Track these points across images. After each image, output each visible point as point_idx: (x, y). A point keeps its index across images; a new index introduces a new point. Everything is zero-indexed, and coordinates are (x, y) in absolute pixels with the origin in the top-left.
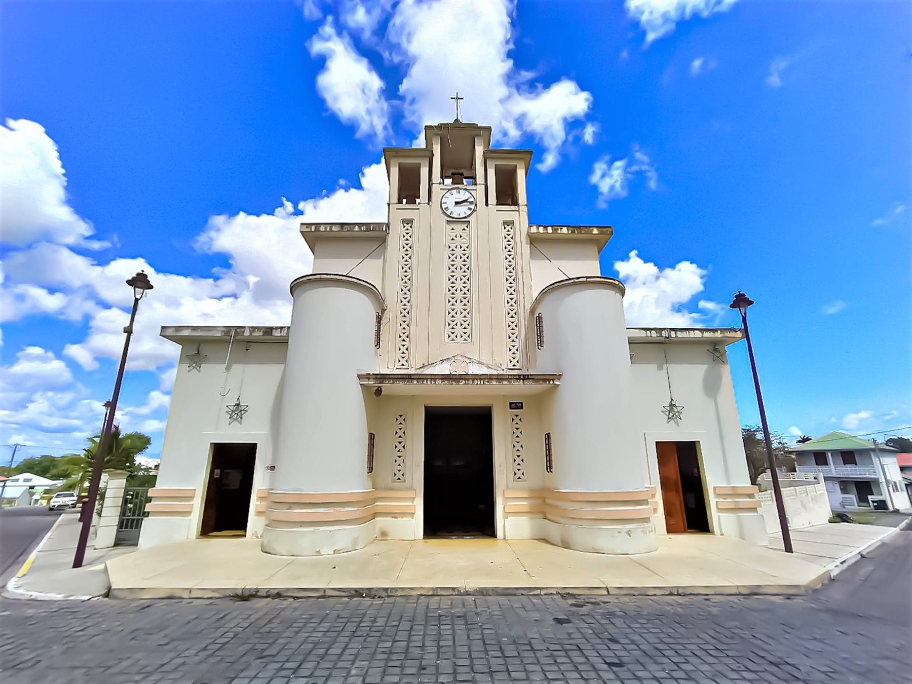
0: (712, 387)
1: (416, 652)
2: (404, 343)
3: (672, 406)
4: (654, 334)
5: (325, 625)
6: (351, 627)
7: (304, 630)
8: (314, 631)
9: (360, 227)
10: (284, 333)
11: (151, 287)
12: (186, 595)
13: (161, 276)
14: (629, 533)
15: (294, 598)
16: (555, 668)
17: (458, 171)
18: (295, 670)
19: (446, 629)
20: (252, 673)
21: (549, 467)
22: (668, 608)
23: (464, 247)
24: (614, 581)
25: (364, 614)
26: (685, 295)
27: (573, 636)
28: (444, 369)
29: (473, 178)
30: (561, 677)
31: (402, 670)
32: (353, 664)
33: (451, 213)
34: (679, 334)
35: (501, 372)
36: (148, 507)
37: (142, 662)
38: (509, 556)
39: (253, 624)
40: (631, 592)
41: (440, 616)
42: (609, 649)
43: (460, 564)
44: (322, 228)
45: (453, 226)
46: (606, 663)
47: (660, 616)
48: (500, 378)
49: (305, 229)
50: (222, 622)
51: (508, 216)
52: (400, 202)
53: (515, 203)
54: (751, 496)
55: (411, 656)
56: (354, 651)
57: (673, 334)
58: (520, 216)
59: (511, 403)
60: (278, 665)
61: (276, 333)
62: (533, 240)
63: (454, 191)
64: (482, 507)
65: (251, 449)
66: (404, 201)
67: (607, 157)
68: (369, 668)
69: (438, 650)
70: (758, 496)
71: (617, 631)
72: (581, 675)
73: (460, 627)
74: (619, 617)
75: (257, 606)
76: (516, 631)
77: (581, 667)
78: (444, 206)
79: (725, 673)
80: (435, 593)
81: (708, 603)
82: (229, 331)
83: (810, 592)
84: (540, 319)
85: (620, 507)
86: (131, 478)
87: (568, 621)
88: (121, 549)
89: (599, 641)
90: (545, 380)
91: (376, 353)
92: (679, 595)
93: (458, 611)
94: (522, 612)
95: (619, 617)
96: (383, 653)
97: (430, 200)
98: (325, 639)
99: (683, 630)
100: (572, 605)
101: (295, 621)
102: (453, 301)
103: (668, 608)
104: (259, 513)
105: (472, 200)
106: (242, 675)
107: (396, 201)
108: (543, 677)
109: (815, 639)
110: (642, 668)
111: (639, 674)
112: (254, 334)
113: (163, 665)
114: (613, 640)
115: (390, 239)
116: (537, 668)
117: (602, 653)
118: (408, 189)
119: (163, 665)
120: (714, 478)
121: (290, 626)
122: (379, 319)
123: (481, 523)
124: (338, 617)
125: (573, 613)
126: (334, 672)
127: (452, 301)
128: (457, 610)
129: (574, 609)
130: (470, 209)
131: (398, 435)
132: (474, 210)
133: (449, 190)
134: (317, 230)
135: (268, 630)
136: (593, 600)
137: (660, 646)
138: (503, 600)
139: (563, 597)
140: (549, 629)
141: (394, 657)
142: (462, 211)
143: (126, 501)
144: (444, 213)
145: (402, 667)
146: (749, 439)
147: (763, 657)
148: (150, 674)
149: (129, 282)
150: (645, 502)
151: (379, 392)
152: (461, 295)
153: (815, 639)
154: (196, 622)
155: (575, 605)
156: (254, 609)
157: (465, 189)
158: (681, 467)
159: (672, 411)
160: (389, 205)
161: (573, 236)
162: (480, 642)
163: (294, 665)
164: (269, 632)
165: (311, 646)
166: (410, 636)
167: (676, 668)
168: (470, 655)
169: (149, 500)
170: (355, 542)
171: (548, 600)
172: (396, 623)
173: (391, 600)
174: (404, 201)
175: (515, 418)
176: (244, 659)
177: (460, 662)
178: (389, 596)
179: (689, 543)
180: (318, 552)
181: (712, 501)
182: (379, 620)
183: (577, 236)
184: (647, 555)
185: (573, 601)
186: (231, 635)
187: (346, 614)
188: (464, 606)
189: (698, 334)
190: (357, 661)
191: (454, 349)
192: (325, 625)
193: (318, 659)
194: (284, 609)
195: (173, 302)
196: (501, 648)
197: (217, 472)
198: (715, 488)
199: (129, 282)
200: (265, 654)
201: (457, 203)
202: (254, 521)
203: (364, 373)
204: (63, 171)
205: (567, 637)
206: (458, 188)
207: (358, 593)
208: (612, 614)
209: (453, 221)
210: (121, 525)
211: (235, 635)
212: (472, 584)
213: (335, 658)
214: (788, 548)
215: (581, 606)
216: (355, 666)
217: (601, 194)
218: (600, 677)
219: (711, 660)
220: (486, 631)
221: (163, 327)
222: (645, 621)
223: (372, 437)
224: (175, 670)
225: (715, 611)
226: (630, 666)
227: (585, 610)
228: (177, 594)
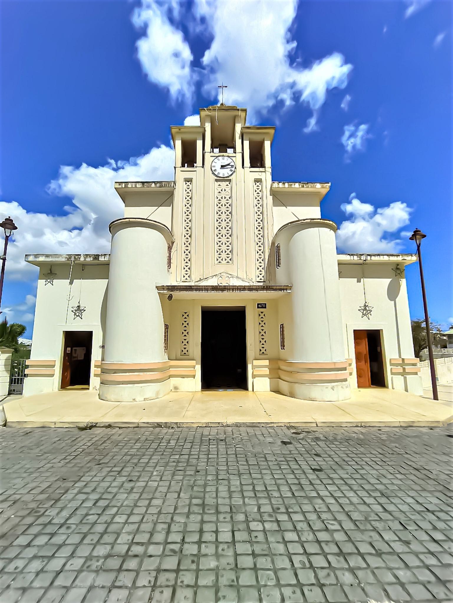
1: (194, 461)
2: (187, 264)
5: (138, 445)
6: (154, 445)
7: (125, 447)
8: (131, 448)
9: (156, 184)
10: (107, 259)
11: (16, 228)
12: (53, 426)
13: (31, 215)
14: (333, 388)
15: (120, 428)
16: (279, 472)
17: (223, 143)
18: (119, 472)
19: (213, 447)
20: (93, 473)
21: (283, 346)
22: (354, 435)
23: (228, 197)
24: (320, 418)
25: (162, 439)
26: (395, 226)
27: (292, 452)
29: (234, 147)
30: (283, 477)
31: (185, 472)
32: (155, 468)
34: (373, 258)
35: (252, 284)
36: (27, 372)
37: (27, 466)
38: (258, 402)
39: (93, 444)
40: (331, 425)
41: (210, 440)
42: (315, 460)
43: (224, 407)
44: (130, 185)
45: (219, 183)
46: (312, 469)
47: (348, 440)
48: (250, 289)
49: (117, 186)
50: (76, 442)
51: (257, 176)
52: (183, 166)
53: (262, 165)
54: (414, 365)
55: (190, 464)
56: (156, 461)
57: (369, 258)
58: (266, 175)
59: (258, 304)
60: (109, 469)
61: (102, 259)
62: (274, 193)
63: (220, 158)
64: (239, 370)
65: (89, 335)
66: (186, 165)
67: (356, 121)
68: (165, 470)
69: (208, 460)
70: (419, 364)
71: (320, 449)
72: (295, 476)
73: (222, 447)
74: (323, 441)
75: (96, 432)
76: (258, 449)
77: (296, 472)
78: (213, 169)
79: (386, 475)
80: (207, 426)
81: (380, 432)
82: (70, 258)
83: (446, 425)
84: (278, 247)
85: (331, 372)
86: (16, 351)
87: (290, 443)
88: (12, 397)
89: (309, 456)
90: (281, 290)
91: (168, 271)
92: (361, 426)
93: (222, 437)
94: (261, 438)
95: (323, 441)
96: (174, 462)
97: (203, 164)
98: (138, 453)
99: (362, 449)
100: (293, 433)
101: (120, 442)
102: (220, 236)
103: (354, 435)
104: (96, 375)
105: (232, 164)
106: (87, 475)
107: (180, 165)
108: (272, 477)
109: (444, 454)
110: (334, 472)
111: (331, 476)
112: (87, 260)
113: (39, 468)
114: (317, 455)
115: (176, 193)
116: (268, 472)
117: (310, 463)
118: (189, 158)
119: (39, 468)
120: (390, 351)
121: (117, 445)
122: (170, 248)
123: (239, 382)
124: (146, 440)
125: (293, 438)
126: (143, 474)
127: (219, 235)
128: (221, 436)
129: (294, 435)
130: (231, 170)
131: (184, 326)
132: (234, 172)
133: (217, 157)
134: (126, 187)
135: (103, 448)
136: (307, 430)
137: (347, 459)
138: (250, 430)
139: (288, 428)
140: (278, 448)
141: (180, 464)
142: (226, 172)
143: (13, 367)
144: (213, 173)
145: (185, 471)
146: (416, 328)
147: (410, 466)
148: (32, 473)
150: (345, 369)
151: (170, 297)
152: (226, 230)
153: (444, 454)
154: (59, 442)
155: (297, 433)
156: (94, 434)
157: (228, 156)
158: (370, 344)
159: (366, 310)
160: (175, 168)
163: (118, 469)
164: (104, 449)
165: (129, 457)
166: (190, 451)
167: (356, 472)
168: (227, 464)
169: (27, 367)
170: (158, 393)
171: (279, 431)
172: (182, 444)
173: (180, 429)
174: (186, 165)
175: (261, 314)
176: (88, 465)
177: (220, 468)
178: (178, 427)
179: (373, 393)
180: (134, 400)
181: (388, 368)
182: (171, 441)
185: (294, 431)
186: (81, 450)
187: (152, 437)
188: (225, 434)
190: (157, 467)
192: (138, 445)
193: (134, 466)
194: (113, 435)
195: (39, 233)
196: (246, 459)
197: (69, 349)
198: (390, 360)
200: (101, 462)
201: (223, 167)
202: (94, 381)
203: (161, 285)
205: (289, 453)
207: (159, 425)
208: (318, 439)
209: (220, 179)
210: (11, 382)
211: (83, 451)
212: (231, 420)
213: (143, 465)
214: (436, 397)
215: (299, 434)
216: (156, 469)
217: (347, 152)
218: (307, 478)
219: (378, 467)
220: (237, 449)
221: (26, 255)
222: (338, 443)
223: (167, 327)
224: (47, 471)
225: (384, 437)
226: (325, 471)
227: (301, 436)
228: (47, 425)
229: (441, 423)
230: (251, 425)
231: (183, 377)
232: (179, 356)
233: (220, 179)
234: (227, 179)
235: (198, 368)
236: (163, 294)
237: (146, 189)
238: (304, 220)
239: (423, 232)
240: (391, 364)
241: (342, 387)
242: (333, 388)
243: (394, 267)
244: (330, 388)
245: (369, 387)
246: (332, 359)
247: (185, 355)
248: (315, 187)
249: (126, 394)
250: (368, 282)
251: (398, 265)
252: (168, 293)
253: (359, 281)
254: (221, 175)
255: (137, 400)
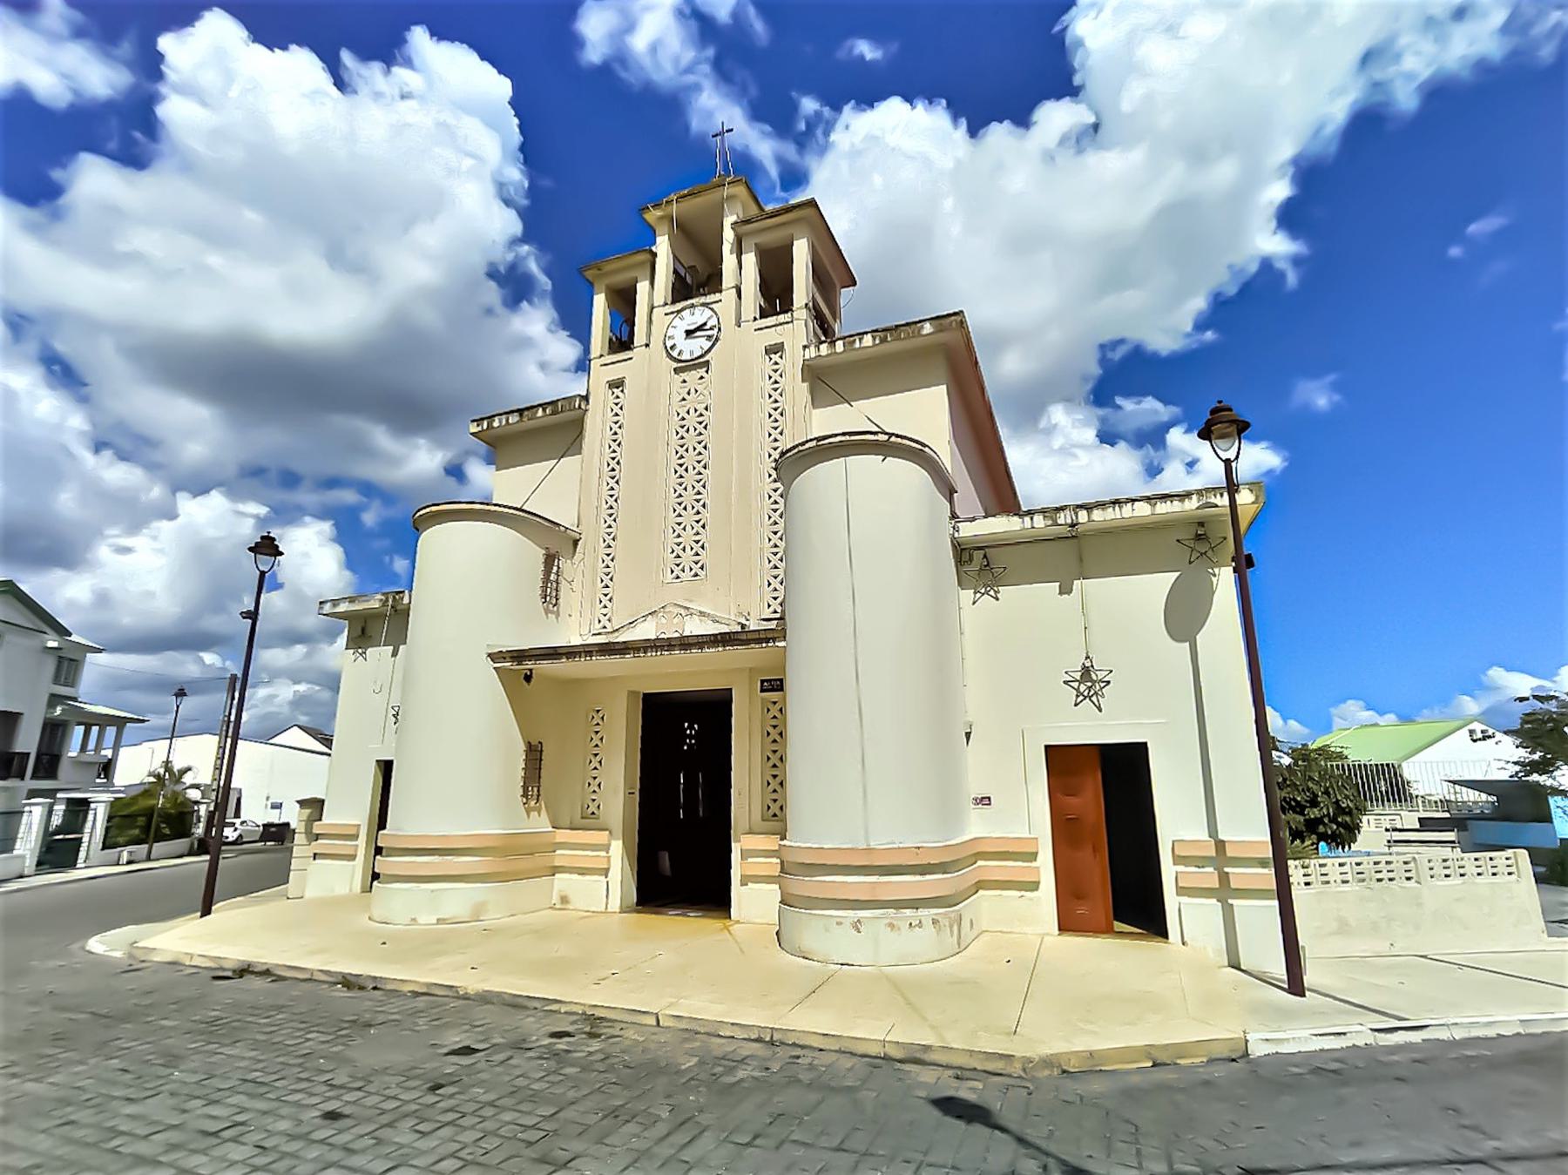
0: (1184, 618)
3: (1086, 672)
4: (1039, 521)
11: (281, 554)
14: (857, 926)
28: (646, 631)
33: (692, 353)
34: (1097, 515)
40: (692, 1031)
45: (684, 376)
51: (772, 337)
57: (1083, 516)
59: (762, 682)
63: (686, 313)
78: (669, 344)
85: (943, 878)
120: (1176, 819)
134: (490, 426)
142: (698, 345)
149: (251, 549)
159: (1088, 683)
161: (885, 347)
162: (1145, 1150)
179: (1115, 956)
183: (892, 346)
184: (1031, 985)
189: (1143, 509)
191: (676, 593)
199: (251, 549)
201: (689, 333)
204: (1406, 99)
206: (693, 306)
209: (684, 366)
214: (1296, 985)
229: (1018, 1066)
230: (511, 1000)
231: (583, 871)
232: (578, 821)
233: (684, 366)
234: (700, 363)
235: (617, 847)
236: (504, 668)
237: (527, 424)
238: (803, 444)
239: (1242, 411)
240: (1177, 860)
241: (891, 926)
242: (857, 926)
243: (1186, 535)
244: (847, 923)
245: (1109, 931)
246: (867, 839)
247: (589, 819)
248: (920, 335)
249: (408, 906)
250: (1094, 589)
251: (1201, 524)
252: (519, 666)
253: (1065, 590)
254: (685, 356)
255: (420, 921)
